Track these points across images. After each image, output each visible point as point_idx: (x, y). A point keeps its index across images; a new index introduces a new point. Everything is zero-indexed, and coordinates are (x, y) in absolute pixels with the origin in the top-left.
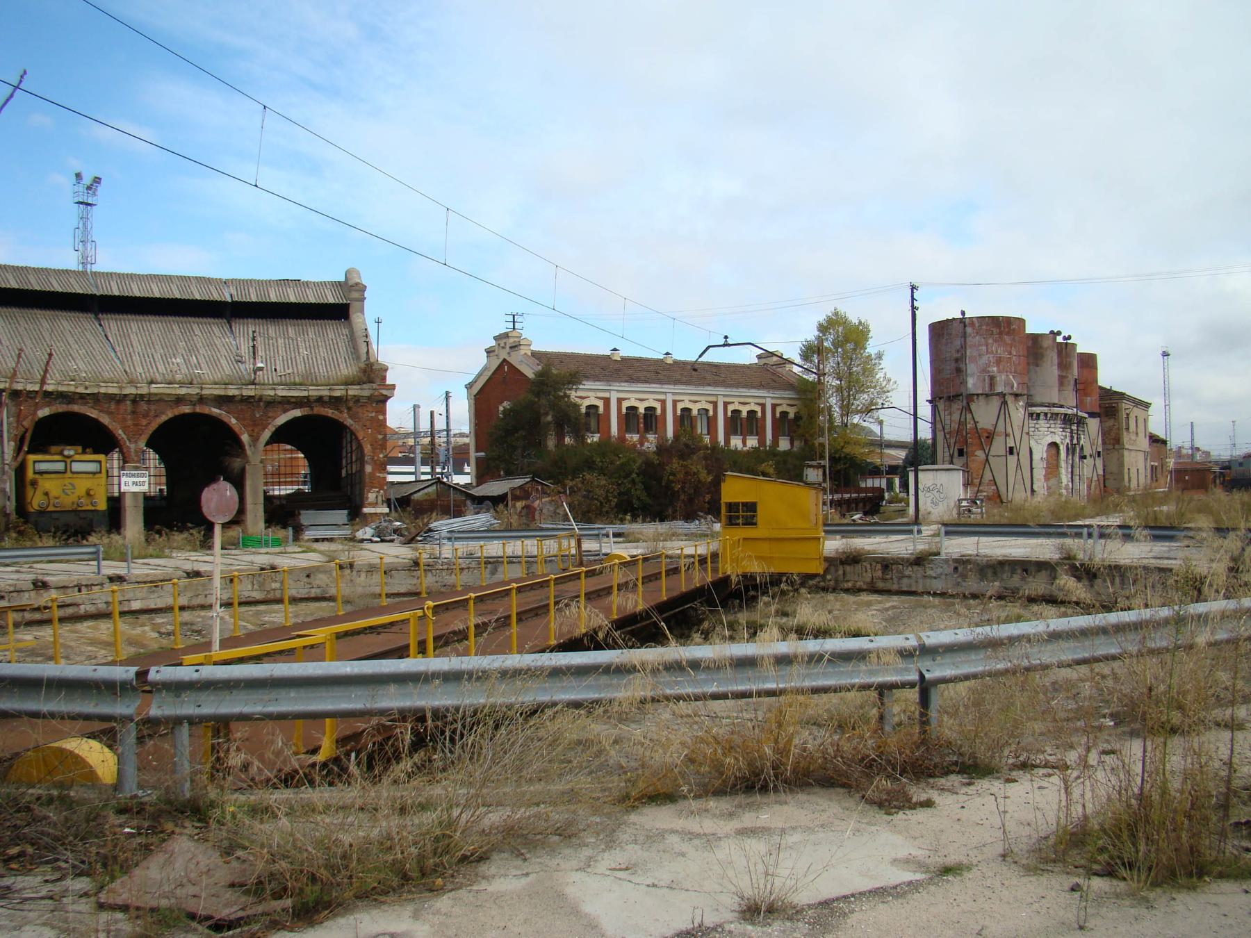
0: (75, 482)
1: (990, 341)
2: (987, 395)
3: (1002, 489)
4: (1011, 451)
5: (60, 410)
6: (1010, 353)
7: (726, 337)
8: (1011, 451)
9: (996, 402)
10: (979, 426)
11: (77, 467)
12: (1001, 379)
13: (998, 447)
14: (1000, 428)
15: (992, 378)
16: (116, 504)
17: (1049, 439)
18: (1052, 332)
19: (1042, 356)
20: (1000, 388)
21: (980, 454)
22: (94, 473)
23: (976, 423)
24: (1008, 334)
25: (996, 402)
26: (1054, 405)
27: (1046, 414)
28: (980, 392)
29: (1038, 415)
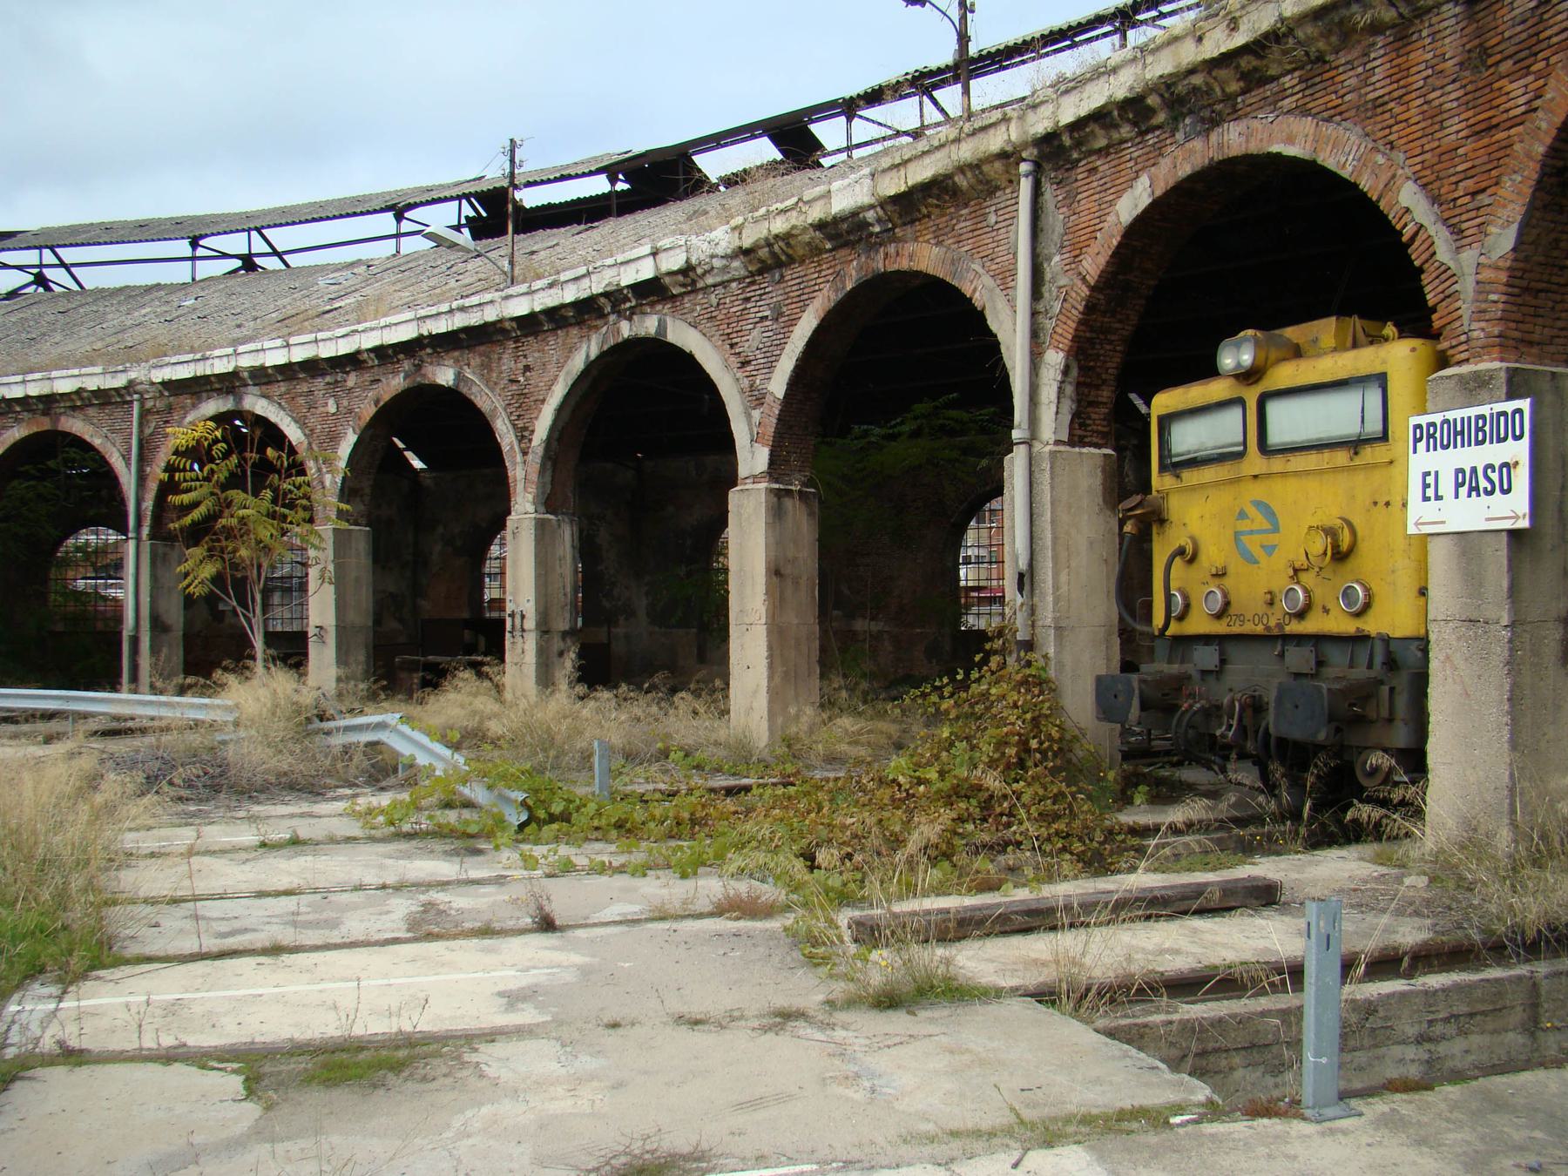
0: (1282, 494)
5: (1185, 170)
11: (1291, 421)
22: (1355, 445)
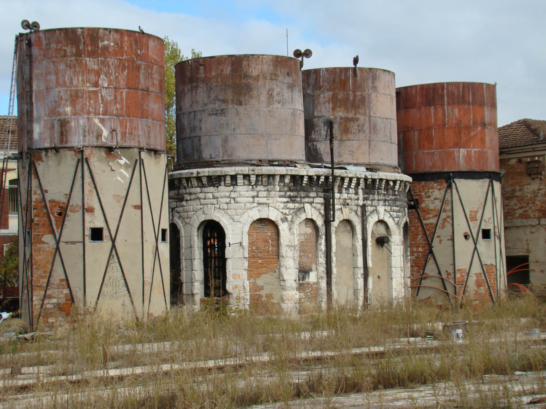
1: (62, 67)
2: (57, 150)
3: (78, 294)
4: (97, 234)
6: (96, 85)
7: (356, 61)
8: (97, 234)
9: (69, 160)
10: (49, 197)
12: (78, 124)
13: (73, 229)
14: (76, 200)
15: (64, 124)
16: (484, 323)
17: (256, 214)
18: (298, 53)
19: (249, 89)
20: (76, 141)
21: (48, 239)
23: (43, 192)
24: (93, 54)
25: (69, 160)
26: (260, 163)
27: (246, 177)
28: (47, 145)
29: (234, 178)
